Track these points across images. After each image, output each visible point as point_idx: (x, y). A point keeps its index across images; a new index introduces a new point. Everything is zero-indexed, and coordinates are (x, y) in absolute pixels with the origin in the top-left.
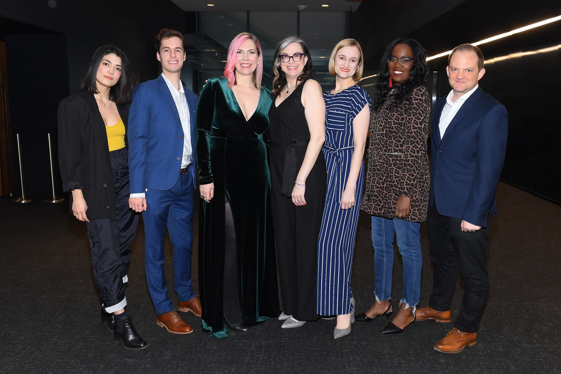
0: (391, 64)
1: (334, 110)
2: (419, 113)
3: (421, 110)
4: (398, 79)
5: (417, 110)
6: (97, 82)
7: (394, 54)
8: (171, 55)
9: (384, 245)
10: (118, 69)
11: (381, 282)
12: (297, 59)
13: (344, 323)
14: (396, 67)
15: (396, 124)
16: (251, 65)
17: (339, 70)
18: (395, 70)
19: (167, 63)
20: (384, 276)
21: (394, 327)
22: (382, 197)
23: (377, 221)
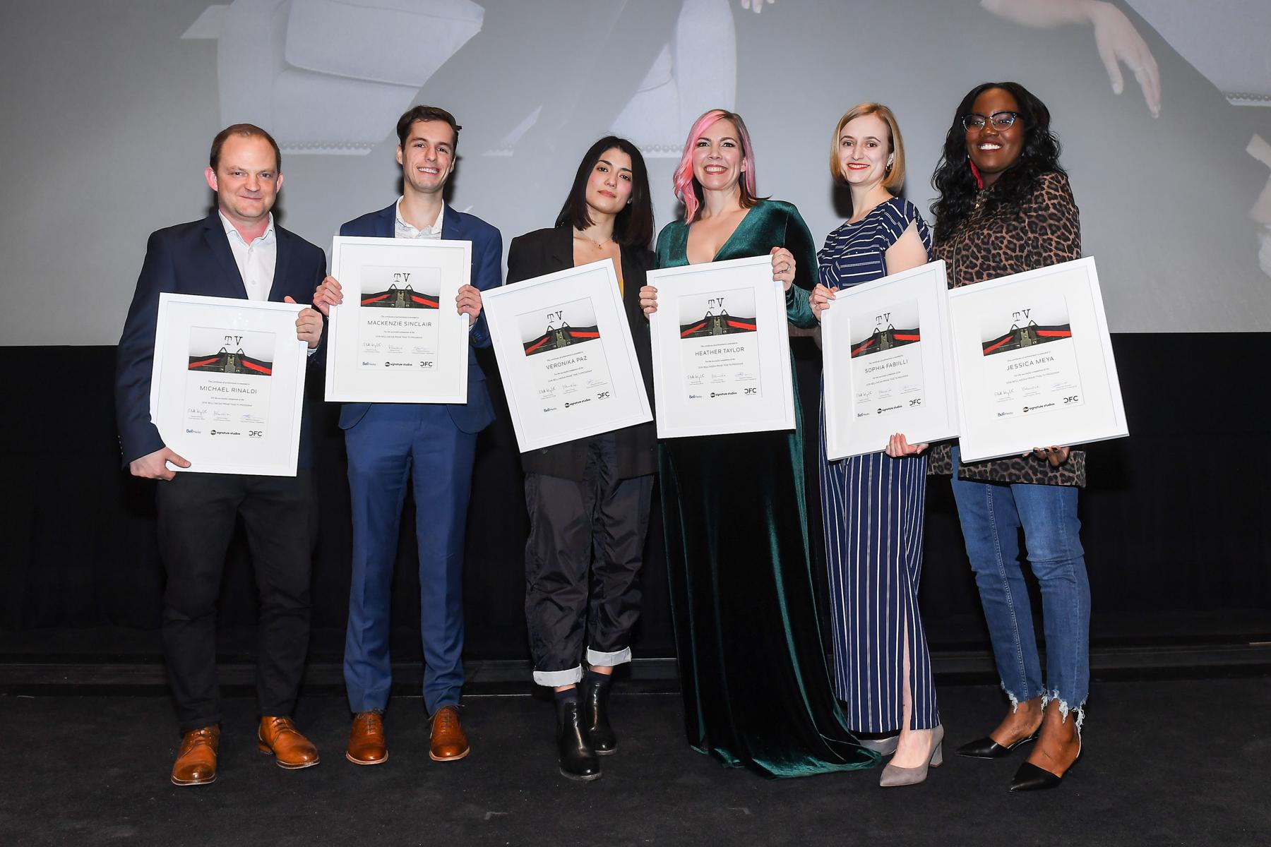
0: (973, 133)
1: (853, 252)
2: (1065, 226)
3: (1068, 219)
4: (991, 162)
5: (1059, 220)
6: (589, 209)
7: (975, 110)
8: (426, 156)
9: (1000, 561)
10: (625, 177)
11: (1011, 657)
13: (913, 753)
14: (986, 136)
15: (1011, 258)
18: (981, 143)
19: (415, 170)
20: (1017, 639)
21: (1037, 771)
23: (974, 508)
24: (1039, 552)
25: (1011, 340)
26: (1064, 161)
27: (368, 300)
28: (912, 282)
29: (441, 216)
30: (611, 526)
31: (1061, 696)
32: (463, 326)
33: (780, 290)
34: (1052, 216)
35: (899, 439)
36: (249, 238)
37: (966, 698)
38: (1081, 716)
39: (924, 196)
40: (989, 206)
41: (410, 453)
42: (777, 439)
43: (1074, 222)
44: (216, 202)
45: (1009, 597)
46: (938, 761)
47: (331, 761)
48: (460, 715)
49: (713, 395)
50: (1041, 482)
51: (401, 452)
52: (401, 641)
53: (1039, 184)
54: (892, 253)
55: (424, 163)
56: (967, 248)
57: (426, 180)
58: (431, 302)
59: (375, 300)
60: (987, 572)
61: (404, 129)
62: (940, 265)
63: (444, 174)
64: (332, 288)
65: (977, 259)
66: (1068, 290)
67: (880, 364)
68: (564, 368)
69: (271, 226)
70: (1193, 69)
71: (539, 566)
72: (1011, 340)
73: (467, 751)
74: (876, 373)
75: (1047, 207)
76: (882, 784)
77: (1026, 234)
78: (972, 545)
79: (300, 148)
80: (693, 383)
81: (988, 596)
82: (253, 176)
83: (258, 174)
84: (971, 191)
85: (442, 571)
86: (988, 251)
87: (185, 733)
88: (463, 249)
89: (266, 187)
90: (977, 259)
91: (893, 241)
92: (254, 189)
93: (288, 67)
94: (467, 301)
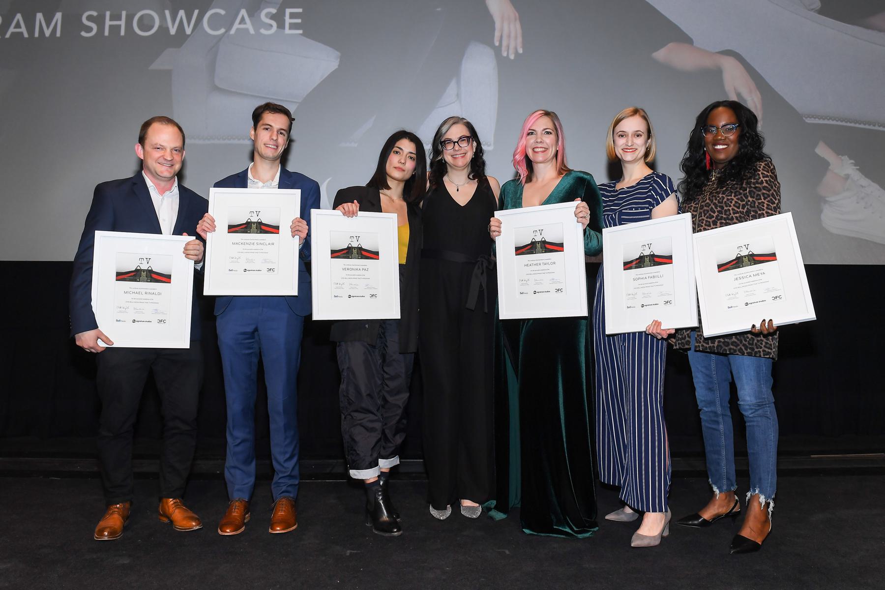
0: (709, 137)
1: (631, 209)
2: (773, 194)
4: (722, 156)
5: (769, 190)
6: (388, 178)
9: (718, 403)
10: (411, 158)
11: (719, 464)
12: (464, 144)
13: (653, 527)
16: (546, 149)
17: (621, 152)
19: (263, 146)
20: (724, 453)
22: (744, 345)
23: (703, 370)
24: (748, 398)
25: (737, 263)
26: (766, 150)
27: (233, 229)
28: (668, 226)
29: (278, 174)
30: (388, 379)
31: (761, 492)
32: (295, 245)
33: (580, 229)
34: (764, 188)
35: (657, 324)
36: (162, 192)
37: (685, 492)
38: (772, 505)
39: (677, 176)
40: (721, 182)
41: (256, 330)
42: (573, 321)
43: (778, 192)
44: (142, 164)
45: (721, 427)
46: (666, 534)
47: (210, 526)
48: (295, 505)
49: (535, 292)
50: (750, 354)
51: (250, 329)
52: (261, 449)
53: (756, 170)
54: (656, 210)
55: (268, 140)
56: (708, 205)
57: (269, 153)
58: (274, 229)
59: (237, 229)
60: (710, 409)
61: (257, 117)
62: (688, 216)
63: (281, 149)
64: (209, 221)
65: (714, 212)
66: (776, 232)
67: (644, 276)
68: (353, 272)
69: (176, 184)
70: (679, 29)
71: (350, 404)
72: (737, 263)
73: (294, 527)
74: (640, 281)
75: (762, 182)
76: (633, 545)
77: (747, 197)
78: (701, 393)
79: (239, 139)
80: (522, 284)
81: (707, 425)
82: (168, 150)
83: (172, 150)
84: (706, 174)
85: (280, 408)
86: (722, 207)
87: (109, 504)
88: (295, 195)
89: (178, 158)
90: (714, 212)
91: (658, 203)
92: (169, 159)
93: (217, 89)
94: (298, 228)
